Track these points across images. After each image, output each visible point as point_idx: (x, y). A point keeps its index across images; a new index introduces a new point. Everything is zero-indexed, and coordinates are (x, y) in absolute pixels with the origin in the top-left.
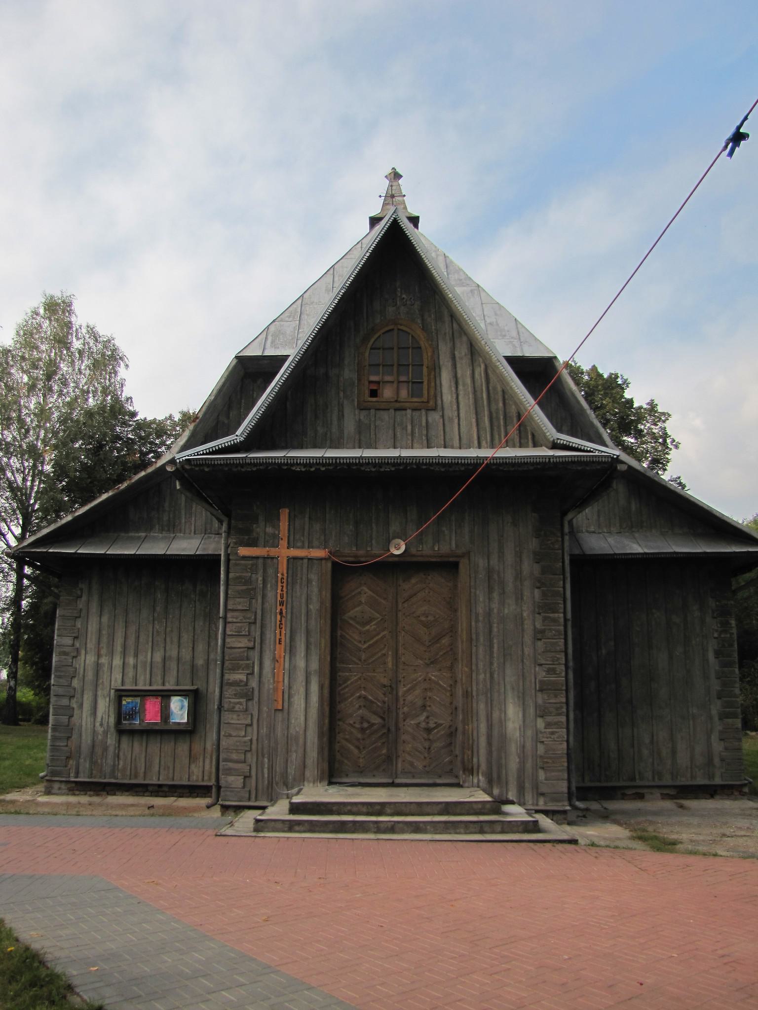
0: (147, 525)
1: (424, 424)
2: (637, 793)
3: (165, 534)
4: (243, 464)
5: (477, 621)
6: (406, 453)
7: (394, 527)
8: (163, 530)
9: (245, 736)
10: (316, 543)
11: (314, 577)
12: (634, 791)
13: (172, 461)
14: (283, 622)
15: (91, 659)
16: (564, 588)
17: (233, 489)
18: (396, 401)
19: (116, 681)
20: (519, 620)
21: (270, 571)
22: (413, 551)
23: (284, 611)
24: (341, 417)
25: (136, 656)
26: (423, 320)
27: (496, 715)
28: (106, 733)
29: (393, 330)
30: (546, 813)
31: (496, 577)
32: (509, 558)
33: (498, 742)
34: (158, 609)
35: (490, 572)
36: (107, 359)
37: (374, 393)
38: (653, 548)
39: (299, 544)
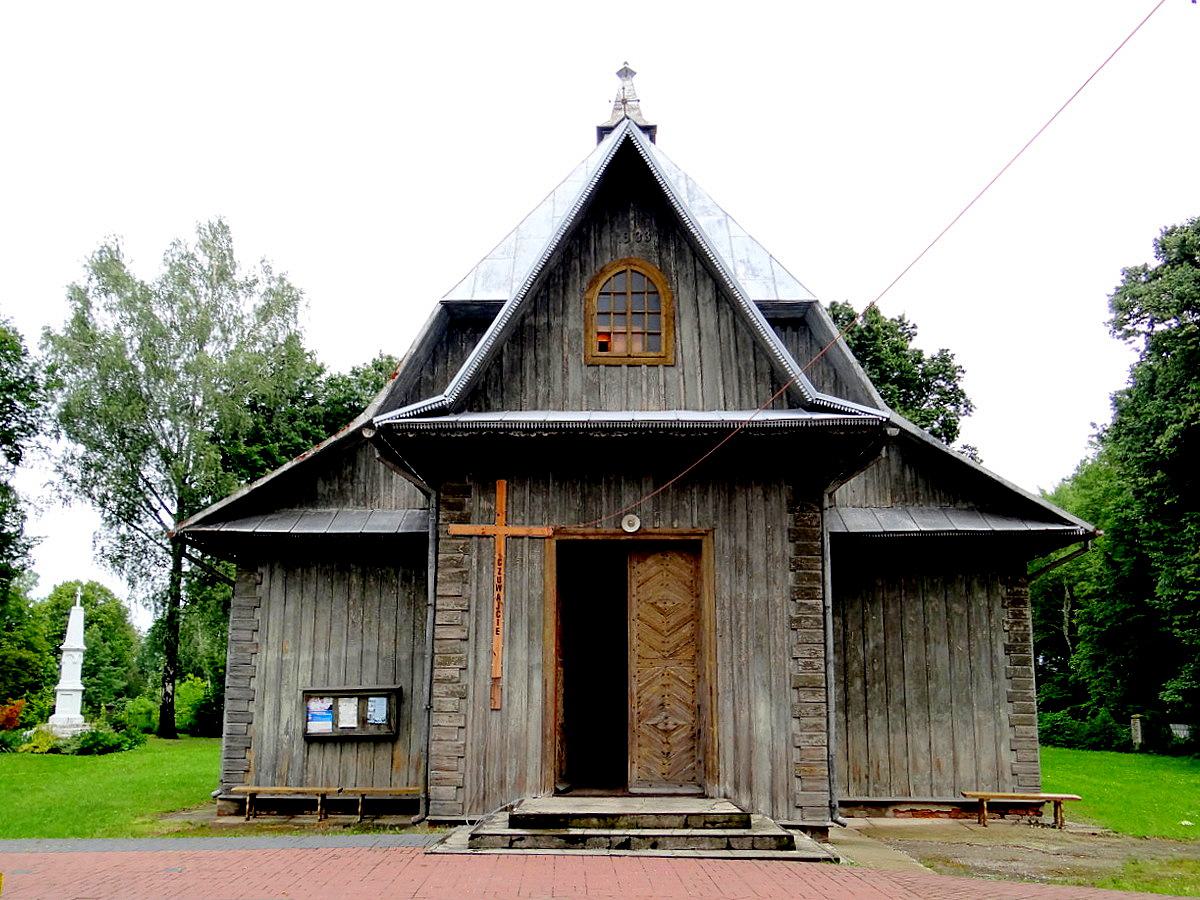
0: (340, 498)
1: (662, 383)
2: (912, 810)
3: (361, 509)
4: (454, 428)
5: (723, 608)
6: (640, 416)
7: (628, 500)
8: (358, 505)
10: (538, 520)
11: (536, 557)
12: (908, 808)
13: (369, 425)
14: (501, 609)
16: (823, 570)
19: (708, 542)
21: (485, 551)
22: (649, 528)
24: (565, 375)
25: (328, 651)
27: (744, 716)
28: (291, 742)
30: (804, 829)
32: (759, 534)
33: (745, 747)
34: (354, 596)
35: (736, 551)
36: (281, 302)
37: (604, 347)
38: (930, 526)
39: (519, 520)
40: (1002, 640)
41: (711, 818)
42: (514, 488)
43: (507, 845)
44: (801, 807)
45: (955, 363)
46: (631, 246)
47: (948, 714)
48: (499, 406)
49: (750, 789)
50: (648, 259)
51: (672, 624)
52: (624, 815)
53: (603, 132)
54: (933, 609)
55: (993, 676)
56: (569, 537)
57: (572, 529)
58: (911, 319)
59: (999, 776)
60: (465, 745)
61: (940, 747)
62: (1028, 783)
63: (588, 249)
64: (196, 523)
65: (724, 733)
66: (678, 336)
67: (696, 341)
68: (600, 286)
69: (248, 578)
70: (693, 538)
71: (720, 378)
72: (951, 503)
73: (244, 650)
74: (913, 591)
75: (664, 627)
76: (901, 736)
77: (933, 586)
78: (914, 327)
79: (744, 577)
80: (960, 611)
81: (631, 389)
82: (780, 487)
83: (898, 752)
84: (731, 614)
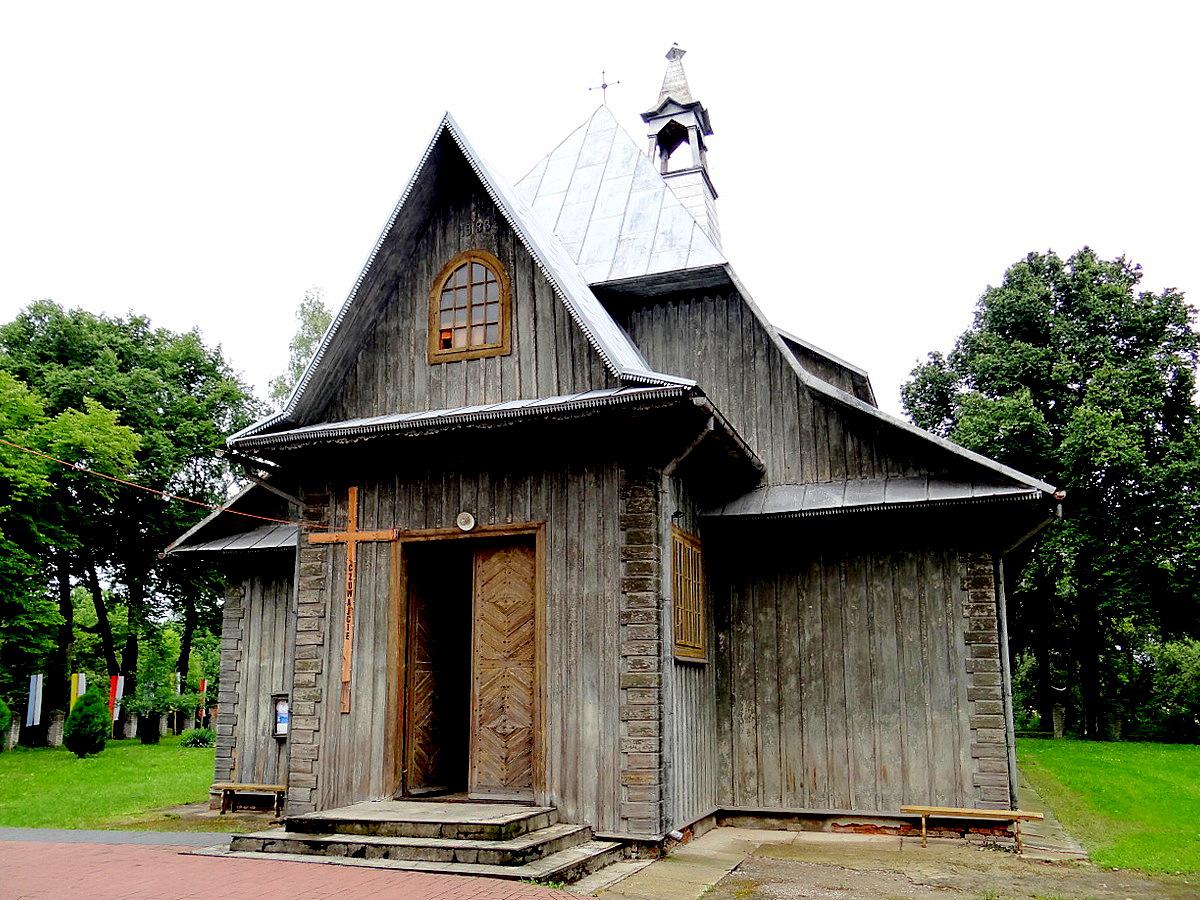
1: (499, 374)
2: (853, 825)
5: (553, 603)
9: (312, 743)
10: (385, 523)
15: (253, 662)
17: (308, 469)
18: (468, 350)
20: (600, 600)
21: (340, 558)
22: (485, 526)
23: (352, 601)
26: (499, 246)
27: (571, 720)
28: (267, 743)
29: (466, 264)
31: (575, 550)
32: (591, 525)
33: (571, 751)
35: (568, 543)
37: (447, 344)
40: (963, 627)
41: (465, 828)
42: (365, 494)
43: (260, 849)
44: (627, 819)
45: (1186, 302)
46: (473, 237)
47: (896, 715)
48: (354, 415)
49: (576, 796)
50: (489, 249)
51: (512, 624)
52: (384, 822)
53: (649, 117)
54: (879, 596)
55: (950, 670)
56: (413, 539)
57: (415, 532)
58: (1132, 259)
59: (958, 786)
60: (319, 747)
61: (887, 753)
62: (992, 797)
63: (434, 247)
64: (180, 545)
65: (551, 738)
66: (514, 323)
67: (532, 326)
68: (442, 286)
69: (234, 591)
70: (526, 532)
71: (554, 361)
72: (899, 472)
73: (231, 658)
74: (853, 576)
75: (506, 627)
76: (795, 740)
77: (879, 568)
78: (1138, 267)
79: (575, 572)
80: (911, 595)
81: (470, 384)
82: (612, 470)
83: (839, 758)
84: (561, 611)
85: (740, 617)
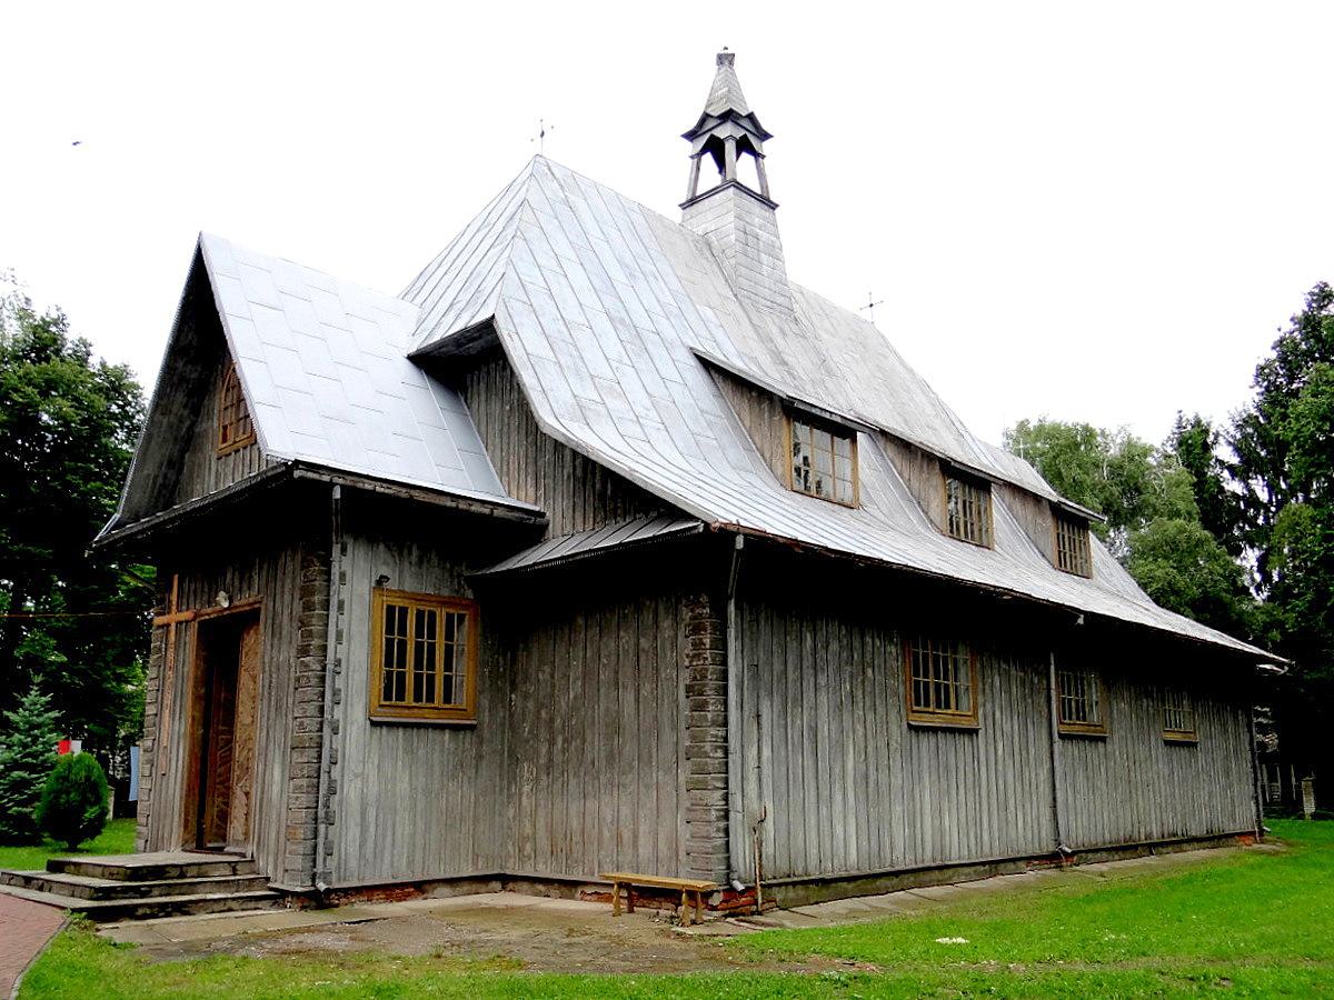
55: (675, 728)
85: (526, 678)
